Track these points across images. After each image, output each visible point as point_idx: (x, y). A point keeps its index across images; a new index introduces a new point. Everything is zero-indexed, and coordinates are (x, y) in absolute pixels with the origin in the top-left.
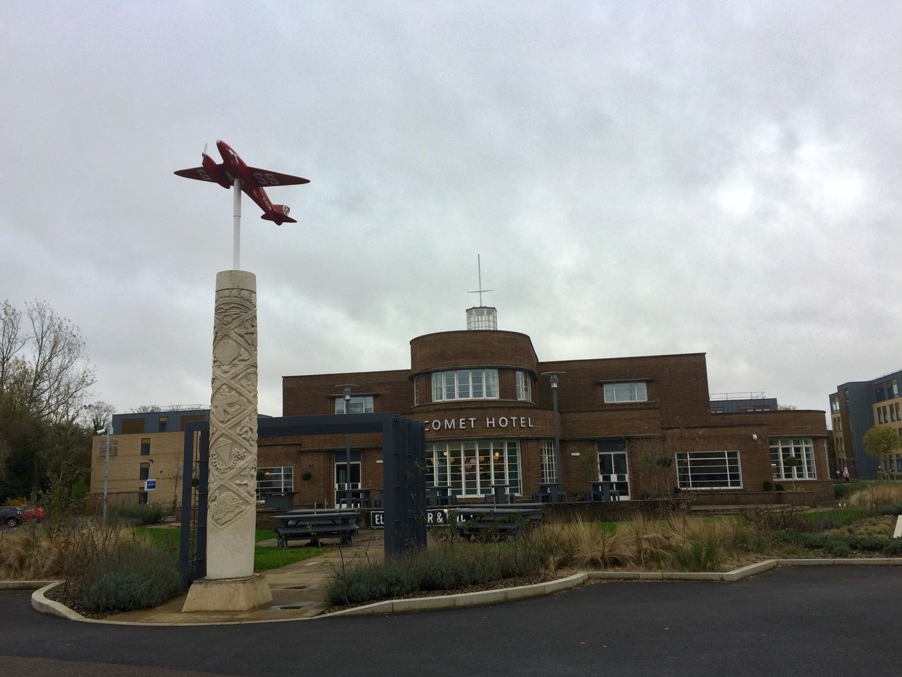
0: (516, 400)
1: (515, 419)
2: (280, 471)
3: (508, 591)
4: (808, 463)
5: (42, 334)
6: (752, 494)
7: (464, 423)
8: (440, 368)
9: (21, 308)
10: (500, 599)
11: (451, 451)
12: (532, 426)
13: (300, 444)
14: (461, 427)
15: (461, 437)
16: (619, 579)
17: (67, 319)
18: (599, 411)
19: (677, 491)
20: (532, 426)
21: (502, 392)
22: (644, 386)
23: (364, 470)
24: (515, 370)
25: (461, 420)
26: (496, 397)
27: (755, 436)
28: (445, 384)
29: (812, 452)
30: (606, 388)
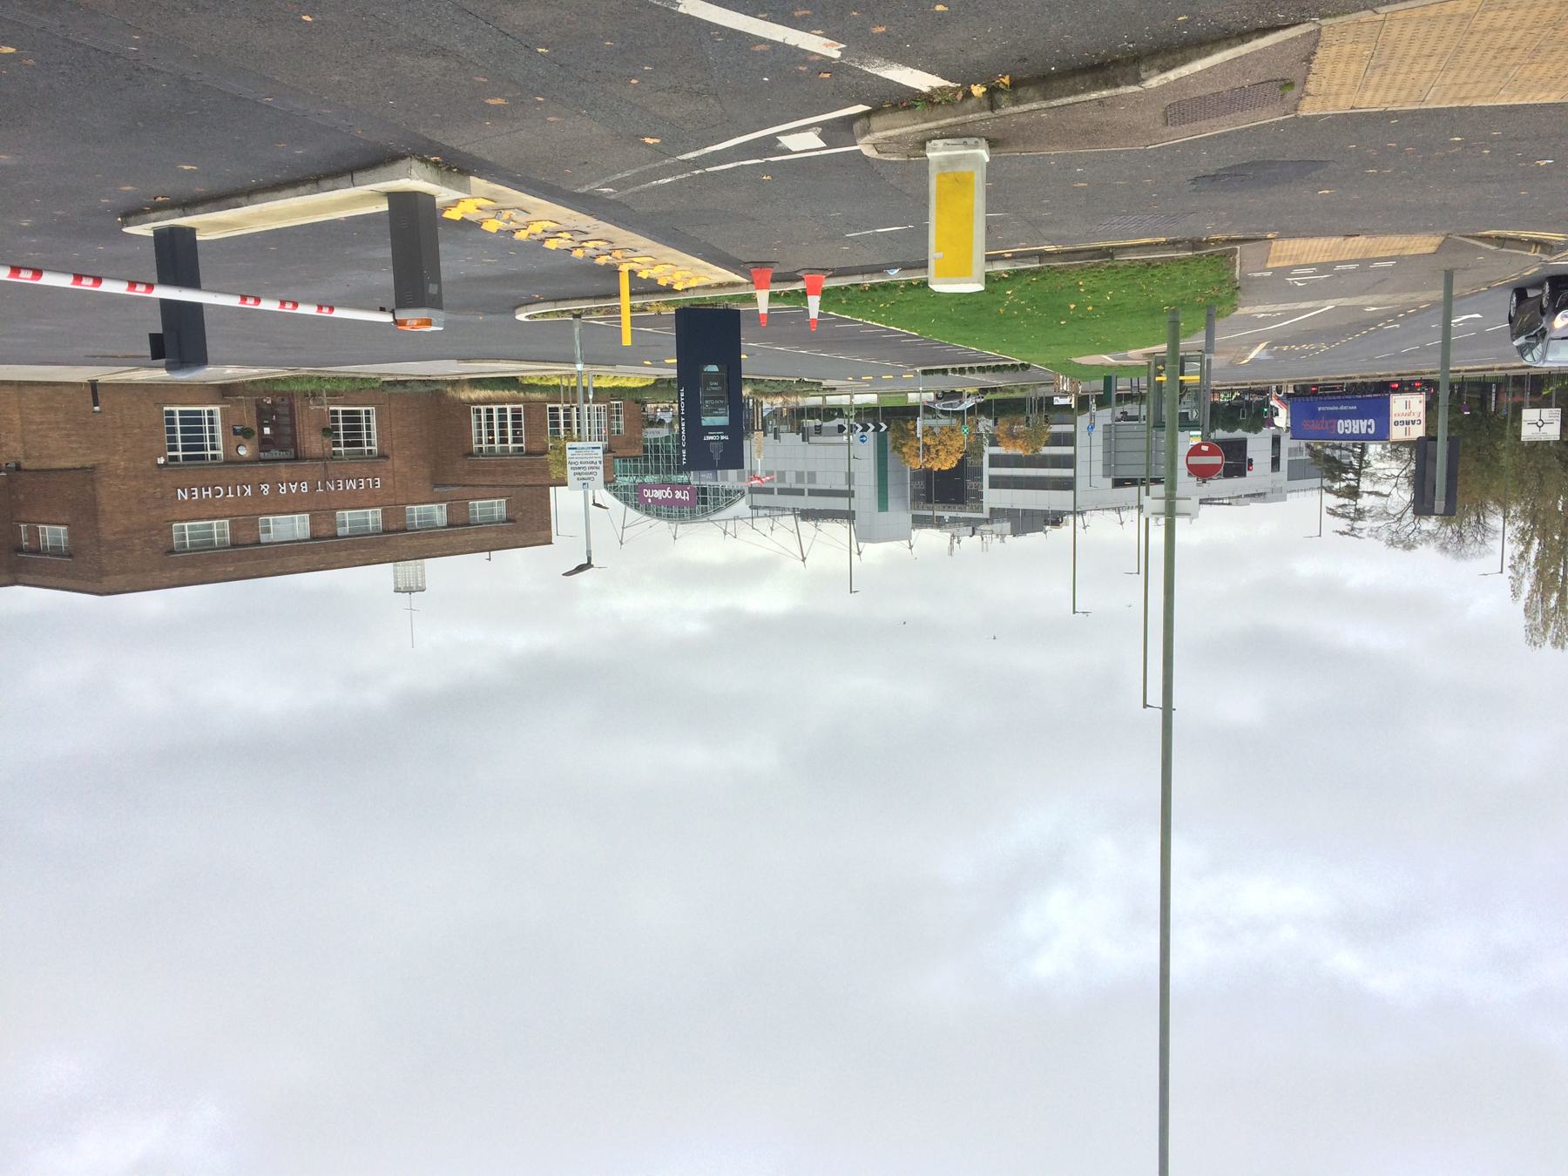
4: (479, 426)
14: (196, 489)
29: (475, 438)
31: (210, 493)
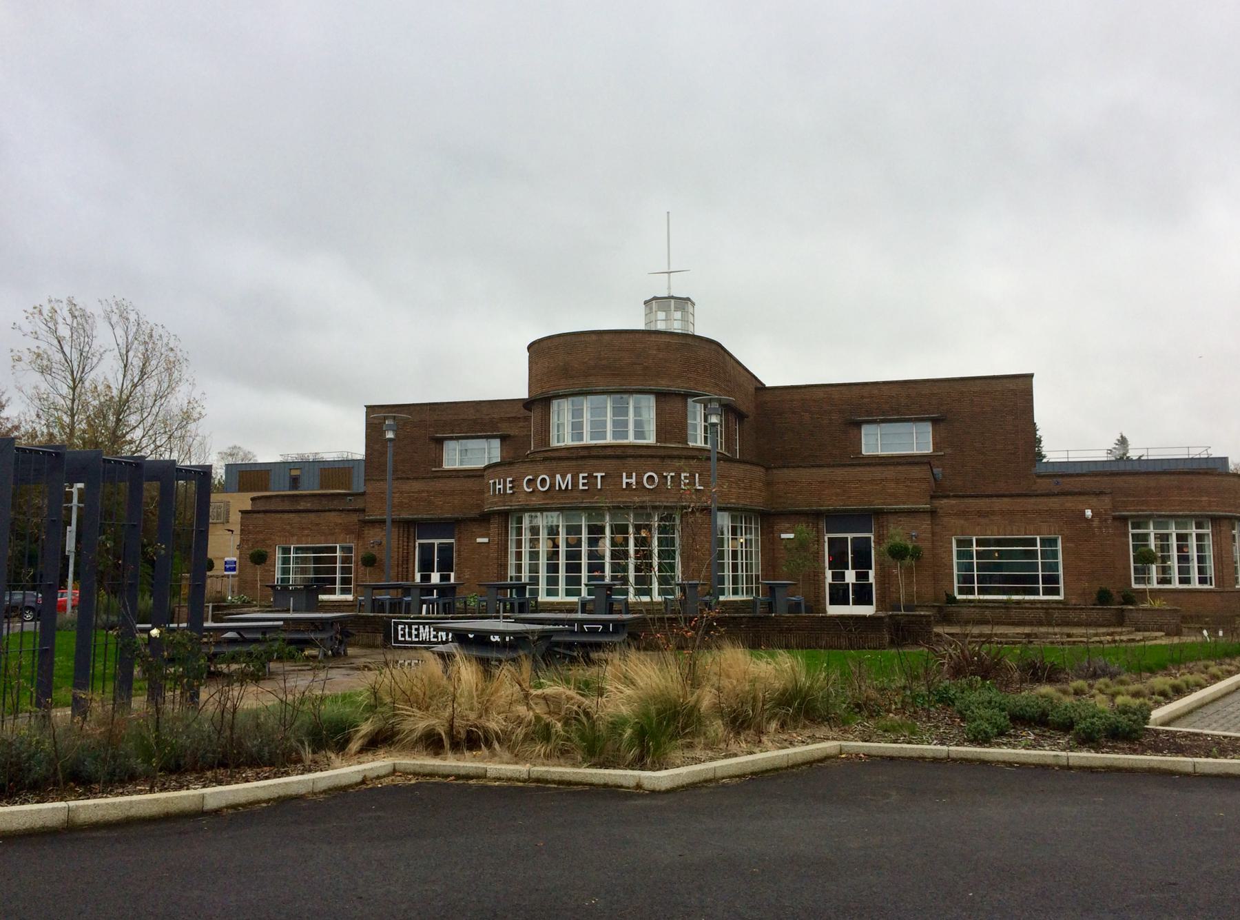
0: (684, 446)
1: (602, 477)
2: (334, 550)
3: (318, 778)
4: (1201, 559)
5: (127, 346)
6: (1075, 609)
7: (586, 481)
8: (561, 392)
9: (93, 308)
10: (49, 824)
11: (588, 525)
12: (702, 488)
13: (363, 511)
14: (581, 487)
15: (582, 502)
16: (448, 776)
17: (160, 325)
18: (829, 466)
19: (951, 599)
20: (702, 488)
21: (661, 432)
22: (927, 428)
23: (459, 551)
24: (685, 396)
25: (581, 475)
26: (651, 440)
27: (1089, 513)
28: (589, 417)
29: (1209, 542)
30: (866, 430)
31: (625, 480)
